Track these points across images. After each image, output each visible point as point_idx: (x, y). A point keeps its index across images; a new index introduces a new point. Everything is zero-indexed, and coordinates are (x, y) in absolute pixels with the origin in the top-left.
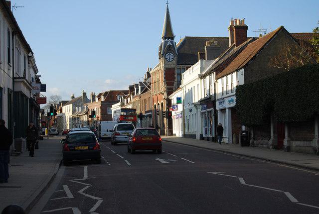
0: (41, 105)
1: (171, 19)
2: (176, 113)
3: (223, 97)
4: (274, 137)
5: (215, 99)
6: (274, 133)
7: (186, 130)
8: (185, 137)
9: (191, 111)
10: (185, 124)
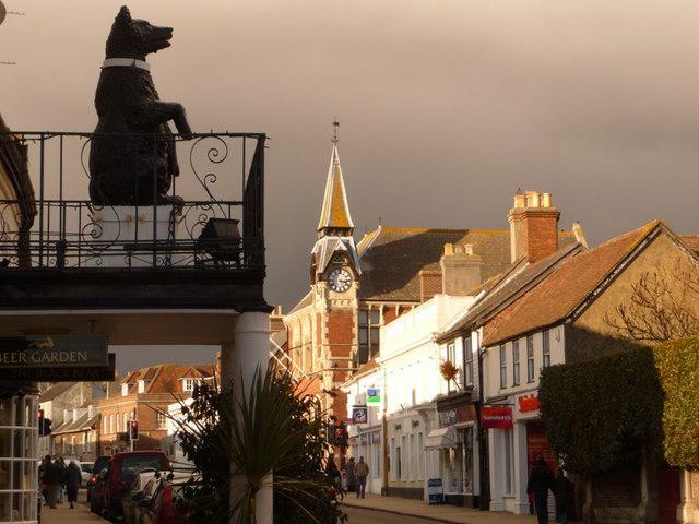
0: (110, 347)
1: (97, 82)
2: (360, 430)
3: (503, 392)
4: (651, 499)
5: (482, 398)
6: (649, 489)
7: (393, 475)
8: (387, 495)
9: (415, 424)
10: (387, 461)
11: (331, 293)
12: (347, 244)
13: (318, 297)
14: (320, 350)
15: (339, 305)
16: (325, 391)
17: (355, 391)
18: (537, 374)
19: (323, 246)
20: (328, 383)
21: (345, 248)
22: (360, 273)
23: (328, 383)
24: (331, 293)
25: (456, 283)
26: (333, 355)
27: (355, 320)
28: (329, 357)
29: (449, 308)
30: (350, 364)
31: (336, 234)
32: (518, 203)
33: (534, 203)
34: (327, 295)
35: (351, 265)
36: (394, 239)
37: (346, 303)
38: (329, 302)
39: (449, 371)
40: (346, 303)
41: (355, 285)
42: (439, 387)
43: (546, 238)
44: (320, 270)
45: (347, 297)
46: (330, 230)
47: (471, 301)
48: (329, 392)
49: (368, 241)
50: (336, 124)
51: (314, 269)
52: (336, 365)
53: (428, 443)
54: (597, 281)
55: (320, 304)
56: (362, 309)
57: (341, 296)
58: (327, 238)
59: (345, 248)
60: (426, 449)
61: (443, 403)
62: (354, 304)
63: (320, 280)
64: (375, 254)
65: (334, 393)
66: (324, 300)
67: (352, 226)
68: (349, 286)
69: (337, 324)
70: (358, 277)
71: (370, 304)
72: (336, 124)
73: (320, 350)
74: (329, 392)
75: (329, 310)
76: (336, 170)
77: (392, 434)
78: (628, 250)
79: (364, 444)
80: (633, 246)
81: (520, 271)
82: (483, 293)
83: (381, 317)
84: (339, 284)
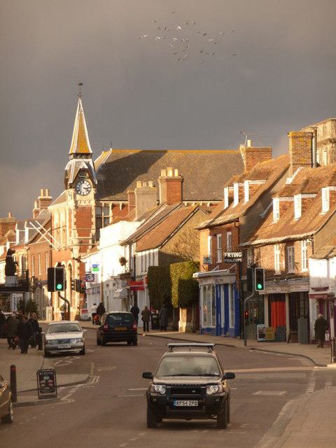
2: (91, 285)
9: (114, 285)
11: (78, 196)
12: (88, 164)
13: (69, 198)
14: (70, 233)
15: (83, 204)
16: (74, 258)
17: (90, 261)
18: (147, 270)
19: (73, 165)
20: (76, 254)
21: (86, 167)
22: (97, 183)
23: (76, 254)
24: (78, 196)
25: (143, 204)
26: (79, 236)
27: (94, 213)
28: (77, 237)
29: (128, 228)
30: (90, 241)
31: (81, 157)
32: (163, 173)
33: (170, 174)
34: (75, 197)
35: (91, 177)
36: (121, 157)
37: (87, 202)
38: (76, 202)
39: (123, 261)
40: (87, 202)
41: (93, 191)
42: (122, 270)
43: (176, 192)
44: (71, 181)
45: (88, 198)
46: (77, 155)
47: (139, 224)
48: (77, 259)
49: (103, 157)
50: (81, 84)
51: (67, 180)
52: (81, 242)
53: (115, 296)
54: (172, 230)
55: (70, 203)
56: (98, 206)
57: (84, 198)
58: (75, 160)
59: (86, 167)
60: (114, 298)
61: (123, 277)
62: (93, 203)
63: (71, 188)
64: (107, 168)
65: (78, 260)
66: (73, 201)
67: (91, 152)
68: (89, 192)
69: (81, 216)
70: (95, 186)
71: (103, 203)
72: (81, 84)
73: (70, 233)
74: (77, 259)
75: (76, 207)
76: (81, 115)
77: (105, 289)
78: (186, 217)
79: (93, 293)
80: (187, 215)
81: (162, 209)
82: (144, 220)
83: (111, 211)
84: (84, 190)
